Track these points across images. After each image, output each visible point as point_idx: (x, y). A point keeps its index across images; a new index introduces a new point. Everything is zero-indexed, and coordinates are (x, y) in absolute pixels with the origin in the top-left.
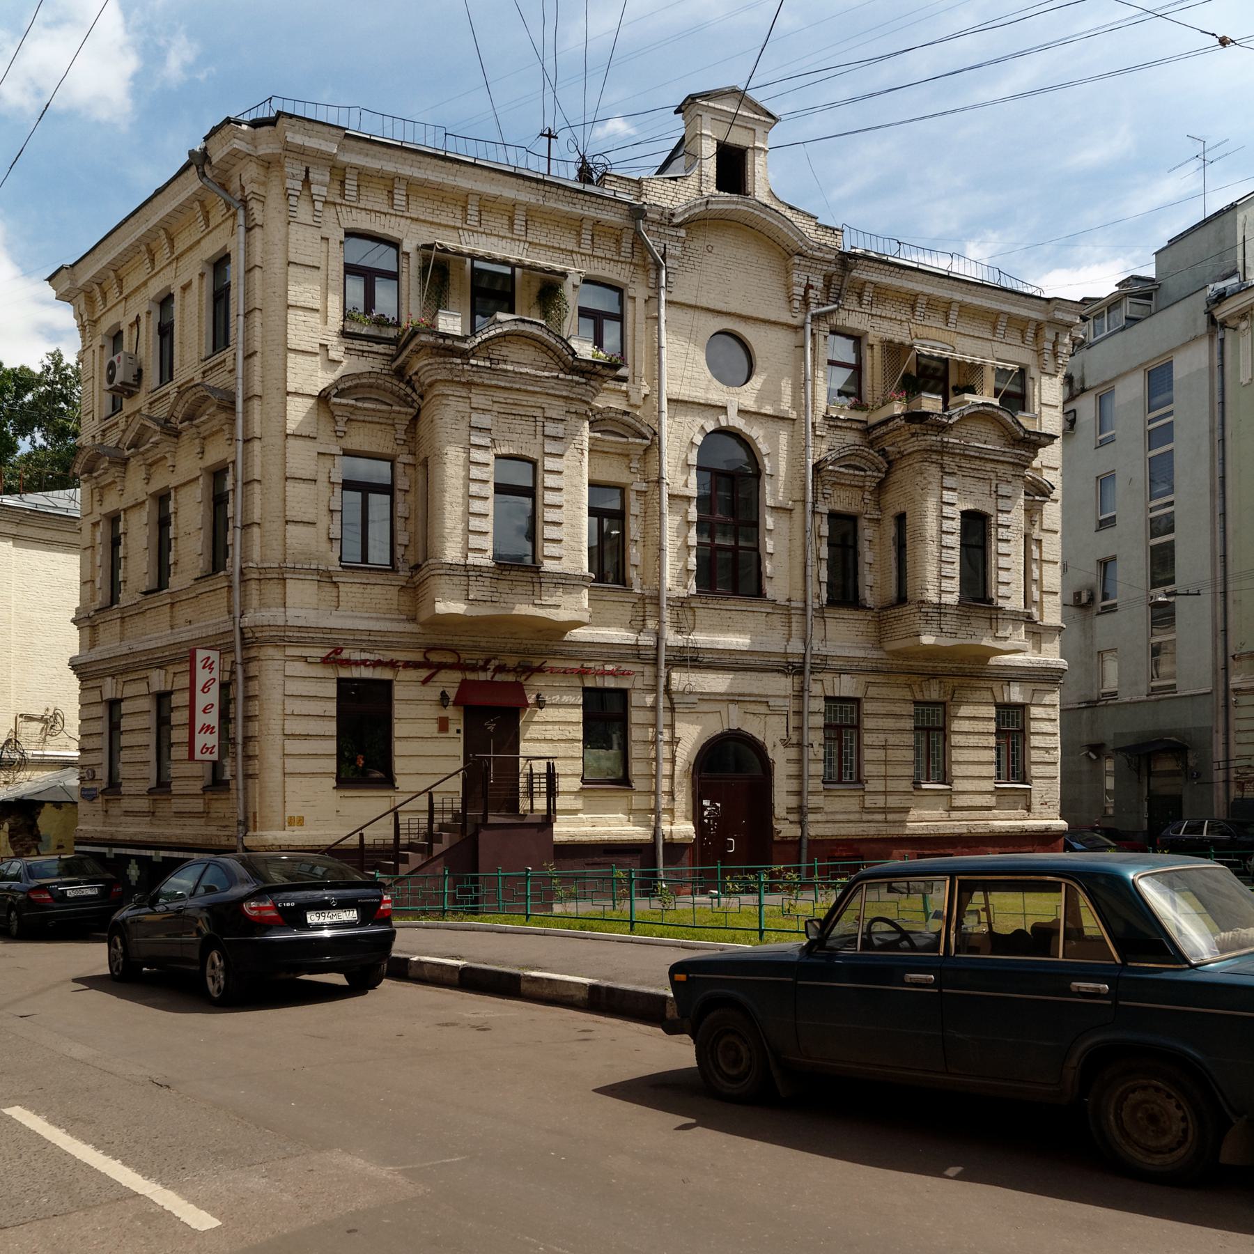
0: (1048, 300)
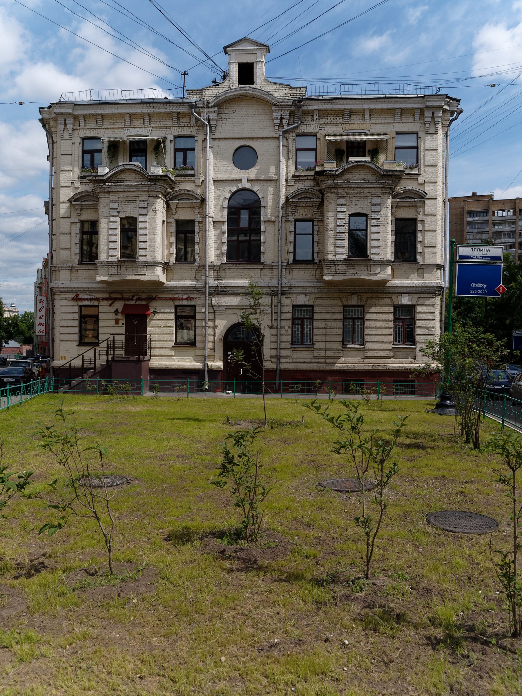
0: (423, 97)
